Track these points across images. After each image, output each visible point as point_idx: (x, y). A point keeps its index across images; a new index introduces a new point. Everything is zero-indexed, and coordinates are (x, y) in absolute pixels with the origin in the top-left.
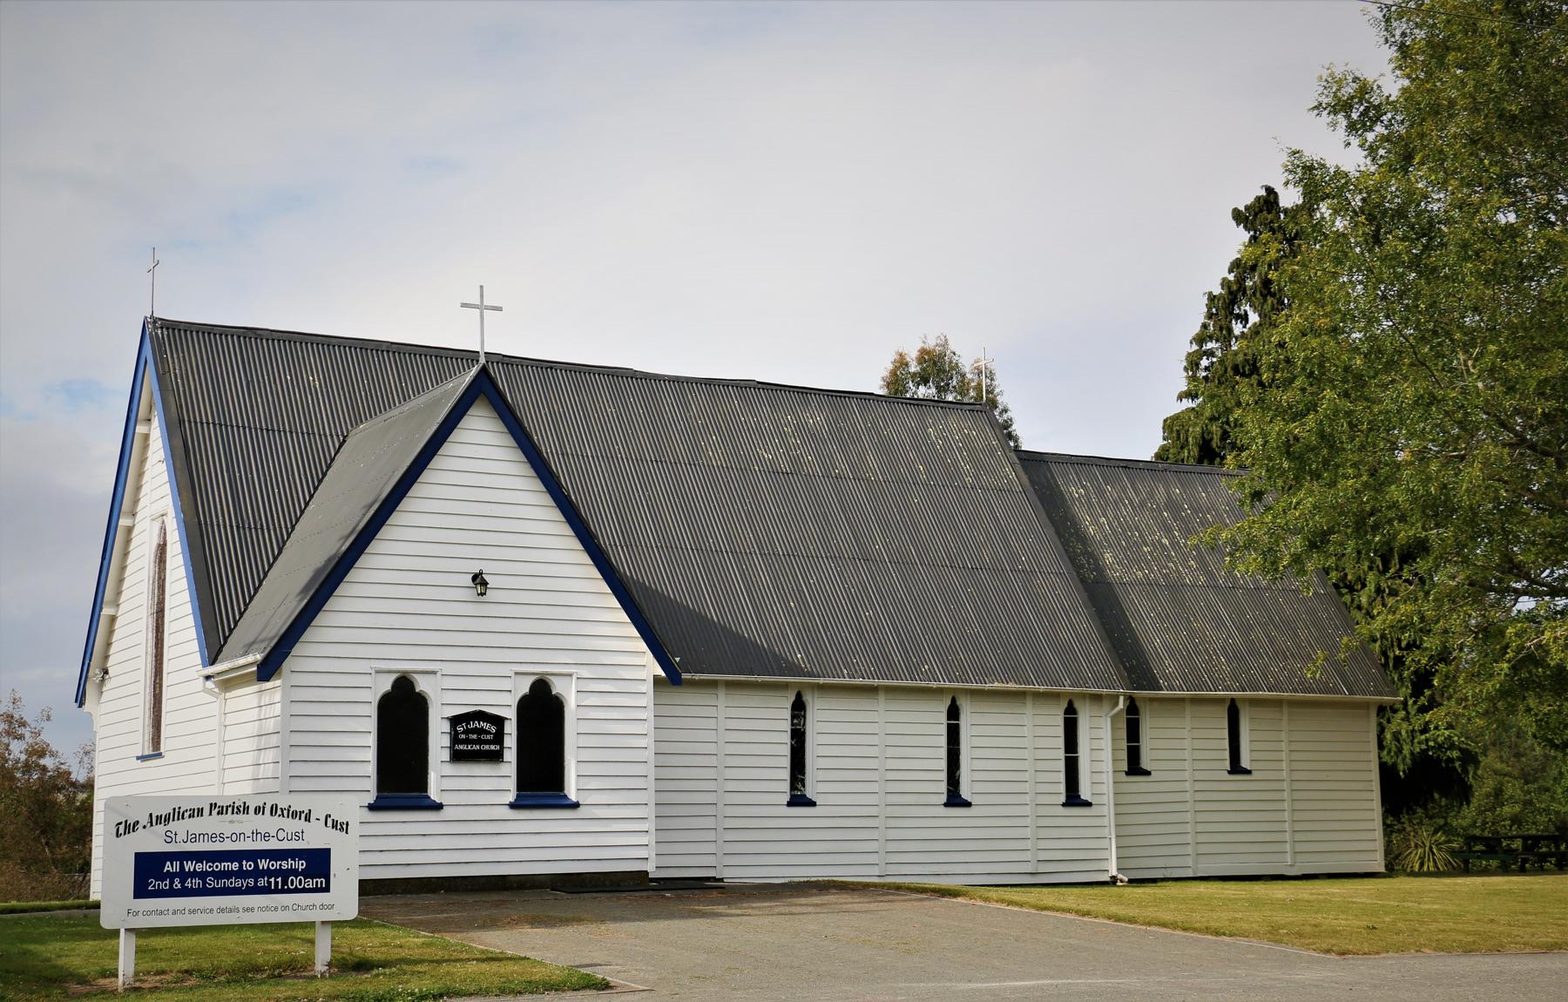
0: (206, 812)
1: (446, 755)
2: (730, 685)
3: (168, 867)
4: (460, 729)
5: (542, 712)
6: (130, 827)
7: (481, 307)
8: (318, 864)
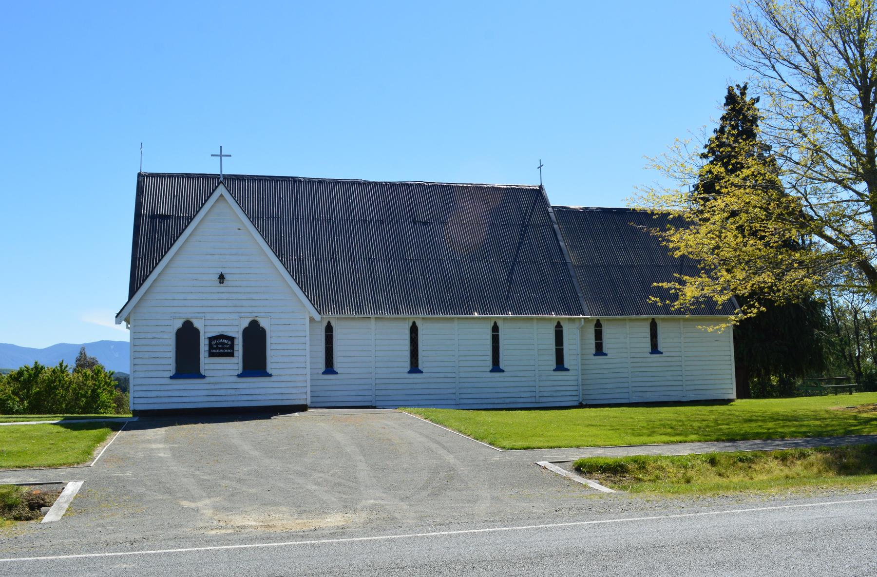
1: (207, 354)
2: (631, 320)
5: (255, 336)
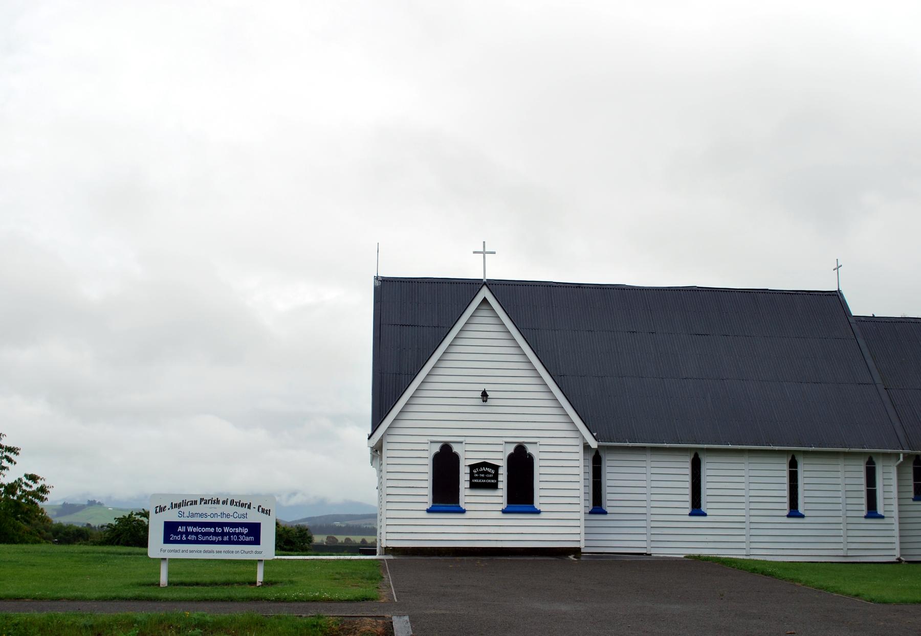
0: (198, 502)
1: (467, 485)
3: (180, 529)
4: (475, 471)
5: (521, 463)
6: (162, 509)
7: (484, 253)
8: (254, 531)
